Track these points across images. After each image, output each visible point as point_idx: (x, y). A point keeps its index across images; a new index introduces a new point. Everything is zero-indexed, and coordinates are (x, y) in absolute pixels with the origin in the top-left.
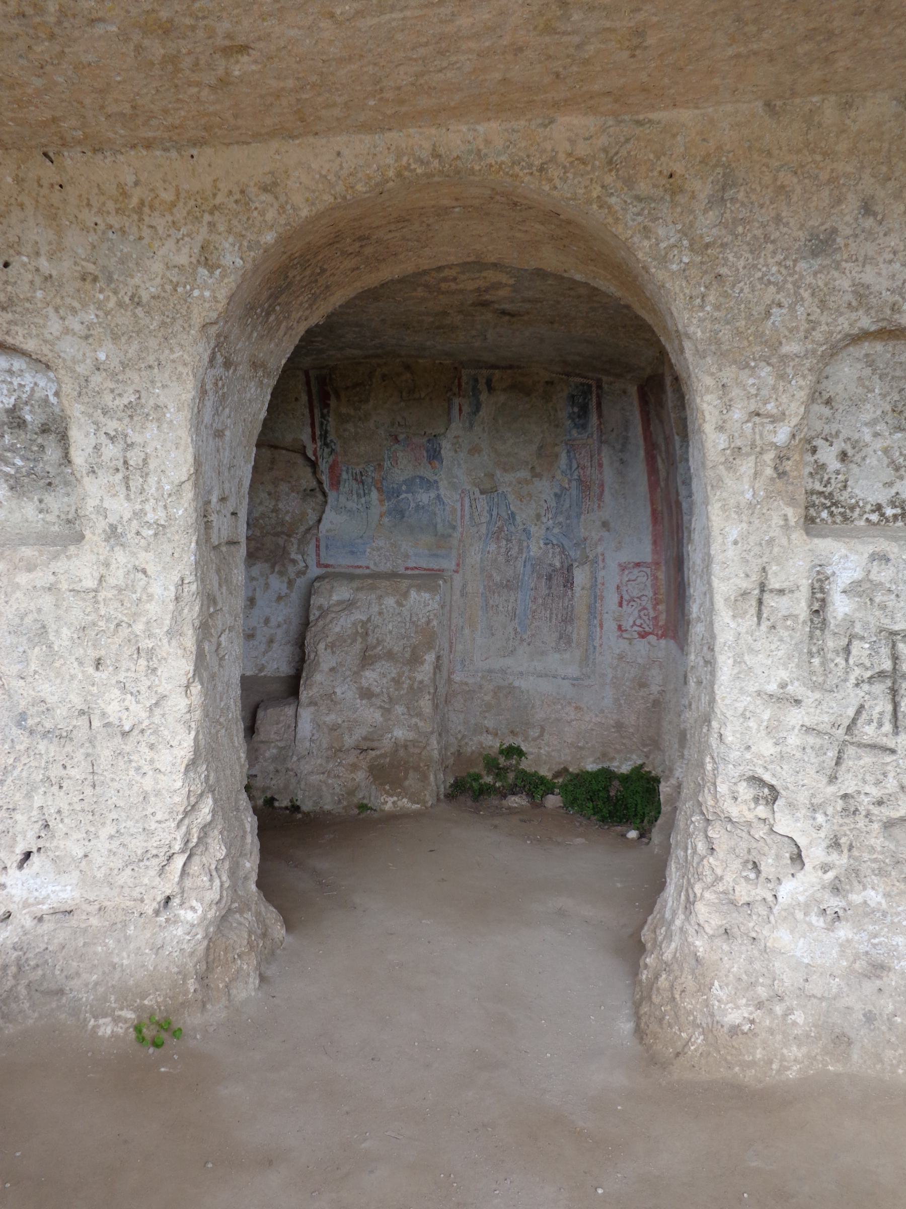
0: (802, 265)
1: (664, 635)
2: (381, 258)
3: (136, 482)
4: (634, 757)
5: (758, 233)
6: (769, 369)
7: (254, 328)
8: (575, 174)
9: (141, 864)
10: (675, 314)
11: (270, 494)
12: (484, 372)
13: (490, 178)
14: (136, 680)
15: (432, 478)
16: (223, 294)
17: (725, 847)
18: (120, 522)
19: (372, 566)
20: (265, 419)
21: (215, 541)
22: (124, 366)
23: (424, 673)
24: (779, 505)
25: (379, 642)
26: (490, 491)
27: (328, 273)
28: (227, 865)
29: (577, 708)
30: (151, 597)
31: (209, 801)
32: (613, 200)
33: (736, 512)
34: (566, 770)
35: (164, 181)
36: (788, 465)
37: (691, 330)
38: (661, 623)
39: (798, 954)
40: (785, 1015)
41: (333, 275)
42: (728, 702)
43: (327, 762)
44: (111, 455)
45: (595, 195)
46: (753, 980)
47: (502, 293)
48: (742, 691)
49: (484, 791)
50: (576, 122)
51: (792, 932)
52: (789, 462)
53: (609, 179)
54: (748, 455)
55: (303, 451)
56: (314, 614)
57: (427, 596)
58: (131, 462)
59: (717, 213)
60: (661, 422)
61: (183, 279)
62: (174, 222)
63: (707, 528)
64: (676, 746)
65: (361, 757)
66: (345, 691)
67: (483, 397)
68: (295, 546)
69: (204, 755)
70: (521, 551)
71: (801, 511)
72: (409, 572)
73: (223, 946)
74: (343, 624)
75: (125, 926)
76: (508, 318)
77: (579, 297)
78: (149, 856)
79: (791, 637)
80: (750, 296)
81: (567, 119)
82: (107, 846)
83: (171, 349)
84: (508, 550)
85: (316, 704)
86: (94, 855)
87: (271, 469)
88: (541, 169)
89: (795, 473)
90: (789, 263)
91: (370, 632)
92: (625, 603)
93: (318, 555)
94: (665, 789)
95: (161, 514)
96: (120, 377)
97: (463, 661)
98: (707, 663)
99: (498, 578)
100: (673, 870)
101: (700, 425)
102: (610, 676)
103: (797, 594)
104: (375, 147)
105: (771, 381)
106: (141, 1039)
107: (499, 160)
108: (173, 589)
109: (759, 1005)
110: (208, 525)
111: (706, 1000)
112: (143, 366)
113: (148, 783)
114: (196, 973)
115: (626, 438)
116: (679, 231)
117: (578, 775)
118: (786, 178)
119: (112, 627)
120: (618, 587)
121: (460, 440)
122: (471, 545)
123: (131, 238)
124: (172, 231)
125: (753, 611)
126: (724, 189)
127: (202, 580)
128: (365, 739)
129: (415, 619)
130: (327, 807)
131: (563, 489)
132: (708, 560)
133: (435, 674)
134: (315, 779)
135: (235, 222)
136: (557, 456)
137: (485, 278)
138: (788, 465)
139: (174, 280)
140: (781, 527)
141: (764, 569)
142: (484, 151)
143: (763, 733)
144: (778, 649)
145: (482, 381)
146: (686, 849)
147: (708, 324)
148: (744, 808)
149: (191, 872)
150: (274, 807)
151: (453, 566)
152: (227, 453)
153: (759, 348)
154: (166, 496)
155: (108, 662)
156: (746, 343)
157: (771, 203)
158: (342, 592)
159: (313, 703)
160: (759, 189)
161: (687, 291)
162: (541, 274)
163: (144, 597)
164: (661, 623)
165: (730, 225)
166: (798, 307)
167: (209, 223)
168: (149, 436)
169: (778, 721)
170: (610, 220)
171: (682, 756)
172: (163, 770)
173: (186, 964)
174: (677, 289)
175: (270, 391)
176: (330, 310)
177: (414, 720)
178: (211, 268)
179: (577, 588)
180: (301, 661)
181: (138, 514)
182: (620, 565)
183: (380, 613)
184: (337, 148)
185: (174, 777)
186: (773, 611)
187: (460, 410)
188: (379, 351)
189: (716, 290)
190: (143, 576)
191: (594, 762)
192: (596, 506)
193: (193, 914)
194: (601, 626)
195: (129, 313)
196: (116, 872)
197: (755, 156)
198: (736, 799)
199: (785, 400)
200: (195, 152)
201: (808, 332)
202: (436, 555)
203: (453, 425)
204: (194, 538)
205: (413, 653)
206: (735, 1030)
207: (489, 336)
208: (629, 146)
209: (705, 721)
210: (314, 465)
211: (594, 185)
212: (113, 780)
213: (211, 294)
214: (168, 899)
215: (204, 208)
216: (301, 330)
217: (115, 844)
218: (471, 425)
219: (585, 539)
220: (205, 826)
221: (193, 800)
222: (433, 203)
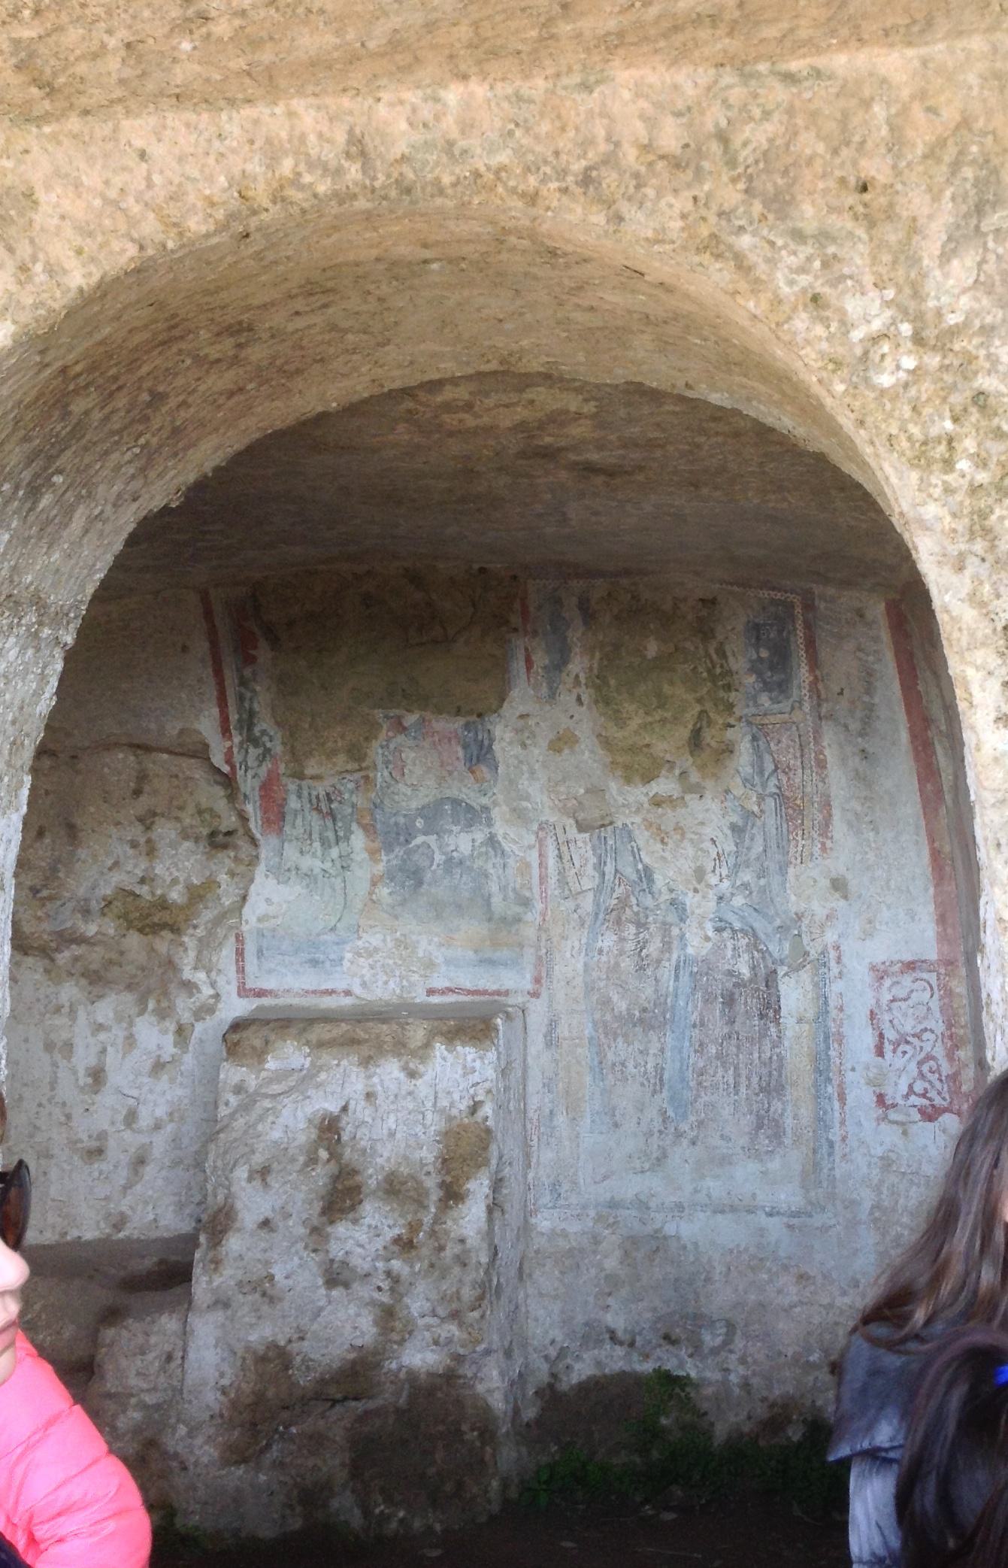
2: (291, 367)
15: (478, 801)
19: (357, 990)
20: (54, 713)
27: (173, 402)
32: (745, 241)
38: (964, 1088)
41: (184, 404)
47: (578, 431)
50: (652, 78)
55: (201, 753)
68: (192, 954)
70: (667, 946)
81: (634, 73)
85: (226, 1305)
88: (587, 180)
92: (888, 1048)
93: (241, 970)
97: (555, 1187)
99: (622, 1005)
102: (867, 1205)
115: (870, 708)
116: (888, 304)
121: (531, 722)
122: (564, 938)
133: (490, 1220)
137: (532, 402)
142: (462, 144)
159: (222, 1303)
162: (638, 392)
179: (788, 1020)
182: (873, 968)
183: (370, 1096)
192: (817, 850)
194: (842, 1098)
202: (492, 963)
203: (515, 693)
210: (228, 782)
216: (128, 520)
219: (799, 917)
222: (375, 253)
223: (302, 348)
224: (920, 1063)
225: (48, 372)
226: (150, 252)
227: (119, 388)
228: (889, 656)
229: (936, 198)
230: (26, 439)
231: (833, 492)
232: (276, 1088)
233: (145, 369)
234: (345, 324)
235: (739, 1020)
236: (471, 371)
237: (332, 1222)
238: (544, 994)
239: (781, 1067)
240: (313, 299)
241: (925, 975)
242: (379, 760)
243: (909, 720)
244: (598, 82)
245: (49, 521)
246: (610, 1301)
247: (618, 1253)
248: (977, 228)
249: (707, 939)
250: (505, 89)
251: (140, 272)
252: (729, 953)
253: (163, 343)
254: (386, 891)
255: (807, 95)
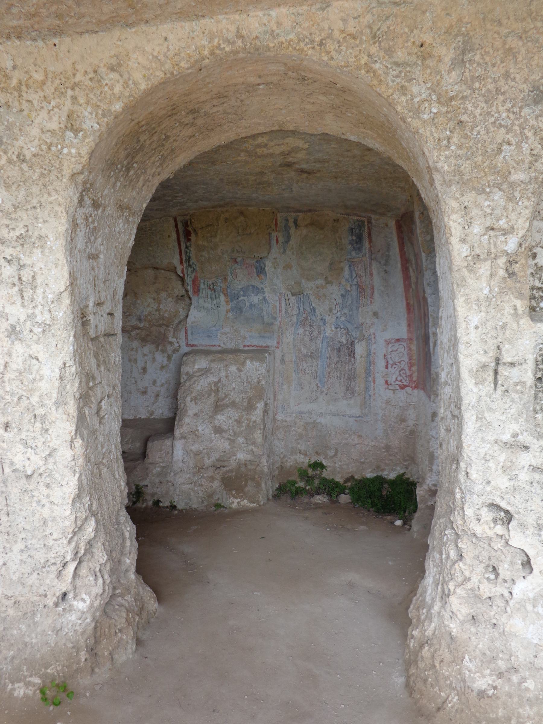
0: (526, 111)
1: (416, 387)
2: (210, 128)
3: (28, 293)
4: (398, 468)
5: (491, 87)
6: (501, 193)
7: (117, 179)
8: (347, 47)
9: (44, 570)
10: (427, 154)
11: (154, 299)
12: (292, 214)
13: (282, 53)
14: (34, 438)
16: (85, 151)
17: (471, 555)
18: (18, 323)
19: (222, 345)
20: (134, 247)
21: (92, 334)
22: (16, 208)
23: (257, 415)
24: (510, 298)
25: (226, 396)
26: (298, 293)
27: (172, 139)
28: (108, 567)
29: (360, 436)
30: (42, 378)
31: (93, 523)
33: (477, 305)
34: (352, 477)
35: (35, 65)
36: (516, 268)
37: (440, 165)
38: (414, 379)
39: (529, 636)
40: (520, 683)
42: (472, 448)
43: (194, 476)
44: (8, 274)
45: (363, 62)
46: (495, 655)
47: (301, 155)
48: (483, 440)
49: (299, 492)
51: (524, 620)
52: (517, 265)
53: (374, 50)
54: (485, 260)
55: (174, 270)
56: (184, 377)
57: (257, 364)
58: (24, 279)
59: (458, 72)
60: (412, 244)
61: (55, 141)
62: (45, 97)
63: (454, 317)
64: (427, 463)
65: (216, 472)
66: (204, 429)
67: (292, 231)
68: (172, 333)
69: (90, 486)
70: (319, 333)
71: (527, 302)
72: (246, 348)
73: (107, 625)
74: (202, 384)
75: (34, 614)
76: (306, 175)
77: (354, 157)
78: (49, 564)
79: (521, 399)
80: (486, 137)
82: (19, 557)
83: (49, 194)
84: (311, 333)
85: (185, 438)
86: (10, 564)
87: (155, 283)
88: (321, 44)
89: (522, 273)
90: (516, 109)
91: (220, 389)
92: (389, 366)
93: (187, 338)
94: (420, 492)
95: (47, 316)
96: (13, 216)
97: (283, 406)
98: (454, 416)
100: (431, 566)
101: (447, 239)
102: (381, 415)
103: (525, 366)
104: (193, 32)
105: (502, 203)
106: (44, 699)
107: (288, 38)
108: (57, 371)
109: (500, 675)
110: (85, 324)
111: (460, 669)
112: (29, 207)
113: (46, 512)
114: (87, 646)
115: (388, 256)
116: (429, 89)
117: (361, 480)
118: (513, 42)
119: (15, 399)
120: (385, 356)
121: (278, 260)
123: (15, 110)
124: (44, 104)
125: (491, 379)
126: (463, 53)
127: (81, 364)
128: (218, 460)
129: (250, 380)
130: (194, 506)
131: (347, 291)
132: (454, 342)
133: (264, 416)
134: (185, 487)
135: (91, 96)
136: (342, 269)
137: (287, 143)
138: (516, 268)
139: (48, 141)
140: (512, 315)
141: (499, 347)
142: (277, 31)
143: (500, 471)
144: (510, 408)
145: (291, 221)
146: (441, 554)
147: (453, 160)
148: (486, 527)
149: (81, 574)
150: (159, 507)
151: (275, 344)
152: (102, 270)
153: (493, 178)
154: (50, 303)
155: (14, 425)
156: (482, 174)
157: (502, 62)
158: (202, 363)
159: (183, 437)
160: (491, 52)
161: (436, 135)
162: (326, 138)
163: (38, 377)
164: (414, 379)
165: (469, 83)
166: (523, 145)
167: (72, 97)
168: (35, 259)
169: (511, 462)
170: (375, 82)
171: (431, 470)
172: (56, 502)
173: (79, 640)
174: (428, 134)
175: (135, 226)
176: (177, 168)
177: (251, 447)
178: (76, 131)
179: (358, 357)
180: (176, 410)
181: (31, 317)
182: (386, 341)
184: (164, 35)
185: (65, 507)
186: (506, 379)
187: (277, 240)
188: (222, 203)
189: (459, 134)
190: (37, 362)
191: (371, 472)
193: (83, 604)
194: (374, 382)
195: (17, 168)
196: (26, 575)
197: (489, 26)
198: (479, 520)
199: (514, 217)
200: (56, 41)
201: (531, 163)
202: (264, 337)
203: (273, 251)
204: (72, 333)
205: (249, 403)
206: (482, 694)
207: (294, 189)
208: (389, 22)
209: (453, 460)
210: (182, 279)
211: (362, 55)
212: (21, 510)
213: (76, 152)
214: (65, 595)
215: (67, 85)
216: (156, 182)
217: (24, 556)
218: (285, 251)
219: (362, 324)
220: (90, 540)
221: (79, 523)
222: (242, 80)
223: (214, 120)
224: (400, 371)
225: (133, 123)
226: (168, 75)
227: (155, 133)
228: (395, 239)
229: (448, 49)
230: (126, 149)
231: (383, 180)
232: (198, 374)
233: (163, 127)
234: (229, 111)
235: (342, 356)
236: (268, 130)
237: (216, 415)
238: (280, 348)
239: (354, 372)
240: (219, 100)
241: (403, 343)
242: (229, 273)
243: (401, 260)
244: (326, 7)
245: (132, 180)
246: (299, 441)
247: (302, 427)
248: (463, 59)
249: (332, 331)
250: (293, 10)
251: (164, 83)
252: (339, 335)
253: (170, 116)
254: (231, 314)
255: (403, 10)
